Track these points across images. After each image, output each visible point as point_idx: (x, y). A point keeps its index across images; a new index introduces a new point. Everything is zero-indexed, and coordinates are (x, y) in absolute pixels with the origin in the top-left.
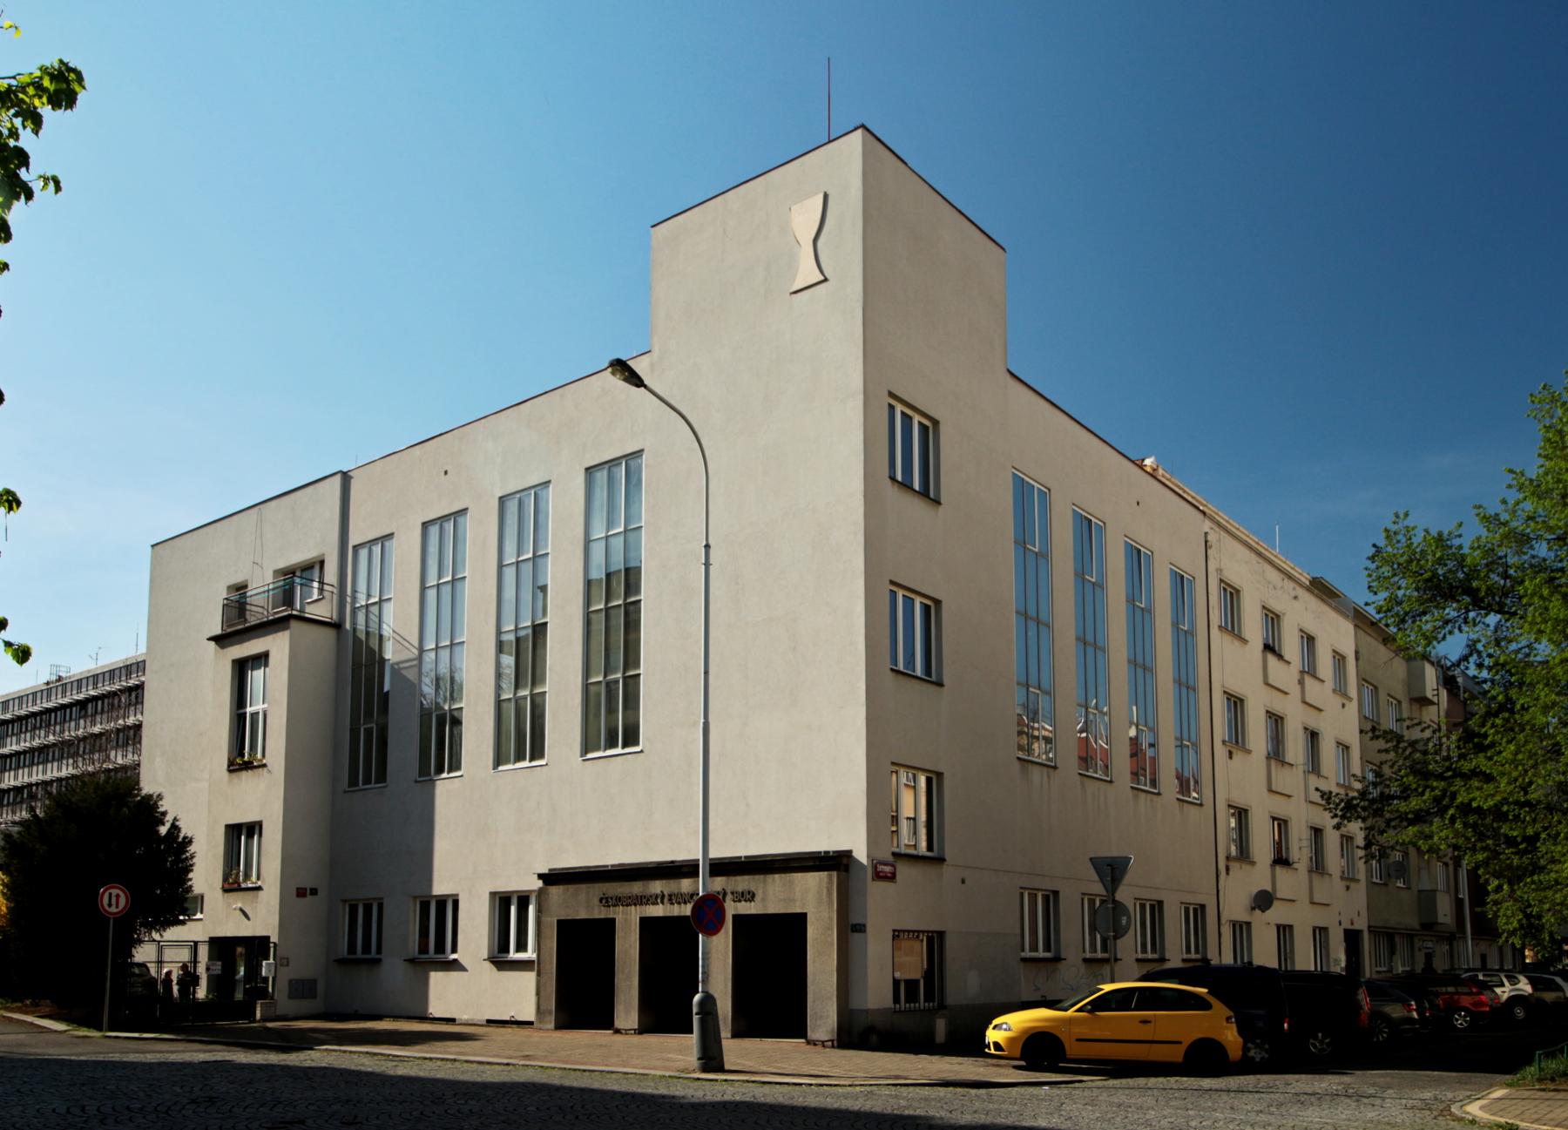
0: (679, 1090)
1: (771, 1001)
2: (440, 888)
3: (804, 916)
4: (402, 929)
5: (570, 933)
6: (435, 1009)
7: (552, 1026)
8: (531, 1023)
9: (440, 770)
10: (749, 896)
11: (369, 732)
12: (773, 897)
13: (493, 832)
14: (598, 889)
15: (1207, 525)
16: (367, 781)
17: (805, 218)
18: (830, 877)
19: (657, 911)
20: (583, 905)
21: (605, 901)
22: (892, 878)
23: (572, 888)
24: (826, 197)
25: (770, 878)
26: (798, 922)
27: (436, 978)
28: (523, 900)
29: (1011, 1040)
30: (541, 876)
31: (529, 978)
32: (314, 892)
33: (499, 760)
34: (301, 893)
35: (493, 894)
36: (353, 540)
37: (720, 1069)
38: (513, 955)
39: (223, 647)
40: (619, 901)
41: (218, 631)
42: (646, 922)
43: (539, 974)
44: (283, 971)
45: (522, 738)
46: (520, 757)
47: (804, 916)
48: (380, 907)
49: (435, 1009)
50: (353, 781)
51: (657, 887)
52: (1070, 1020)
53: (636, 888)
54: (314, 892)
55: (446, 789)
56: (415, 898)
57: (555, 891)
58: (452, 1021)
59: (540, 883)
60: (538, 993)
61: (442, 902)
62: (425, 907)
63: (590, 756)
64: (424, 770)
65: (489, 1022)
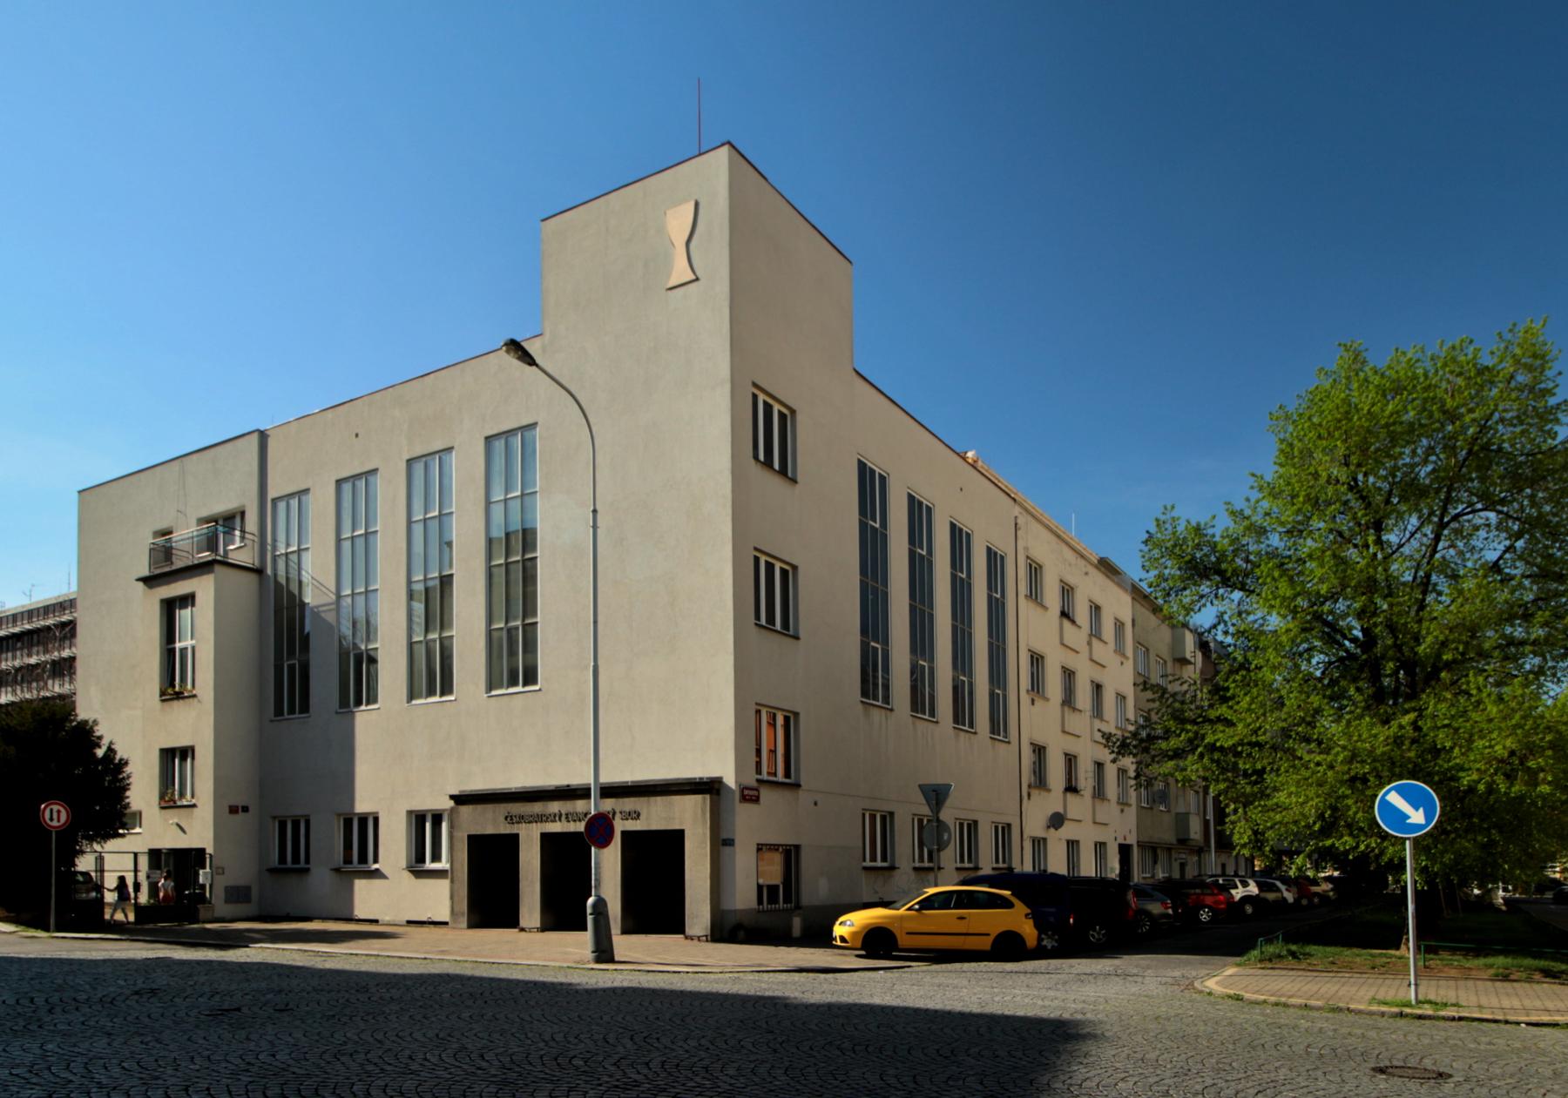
0: (575, 978)
1: (655, 901)
2: (361, 806)
3: (681, 832)
4: (327, 841)
5: (478, 845)
7: (465, 925)
9: (359, 703)
10: (636, 815)
11: (292, 668)
12: (655, 816)
13: (406, 759)
15: (1017, 510)
16: (292, 711)
17: (678, 222)
19: (555, 827)
20: (491, 822)
21: (510, 819)
22: (756, 800)
23: (480, 807)
24: (697, 204)
25: (653, 799)
26: (677, 837)
27: (360, 885)
28: (437, 818)
29: (854, 934)
30: (452, 797)
31: (443, 885)
32: (245, 809)
33: (412, 696)
34: (233, 810)
35: (410, 813)
36: (272, 493)
37: (611, 960)
38: (429, 865)
39: (151, 587)
40: (522, 819)
41: (145, 572)
42: (546, 838)
44: (217, 878)
45: (433, 675)
47: (681, 832)
49: (360, 912)
50: (279, 711)
51: (555, 807)
52: (901, 918)
53: (537, 808)
54: (245, 809)
55: (364, 718)
56: (274, 818)
57: (465, 810)
58: (376, 921)
59: (452, 803)
60: (452, 898)
61: (363, 819)
62: (348, 823)
64: (344, 703)
65: (409, 922)
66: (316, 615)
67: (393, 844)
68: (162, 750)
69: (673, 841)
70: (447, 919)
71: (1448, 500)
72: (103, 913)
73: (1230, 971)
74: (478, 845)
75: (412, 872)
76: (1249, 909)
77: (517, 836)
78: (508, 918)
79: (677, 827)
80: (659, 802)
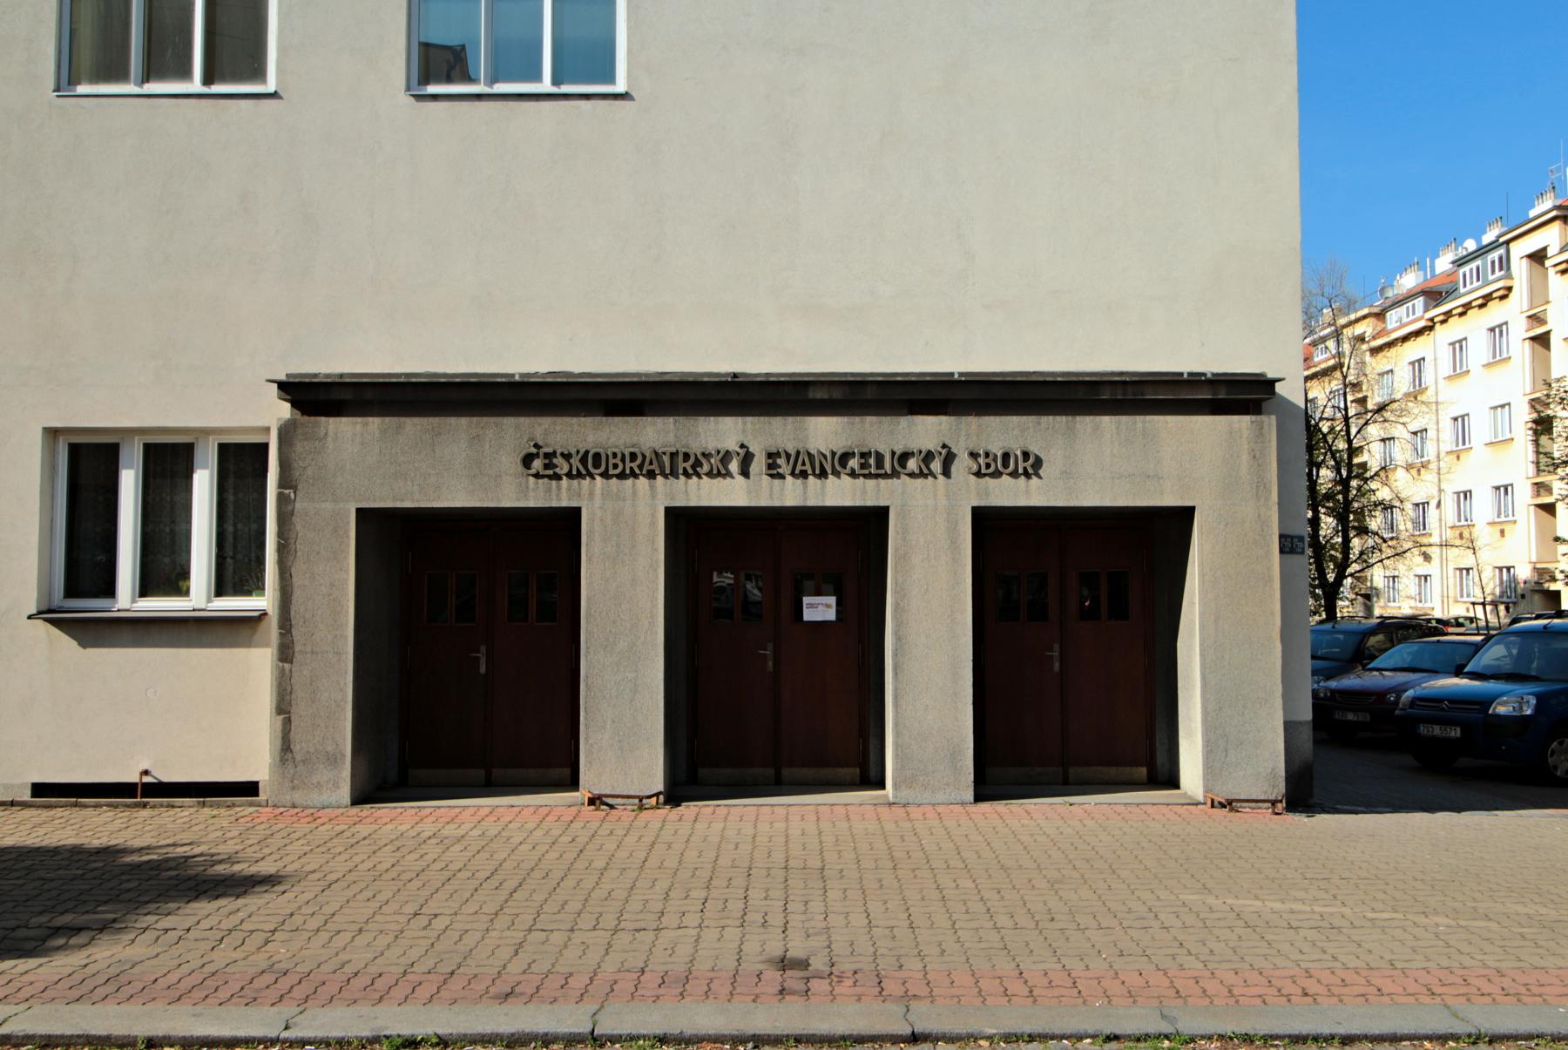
5: (398, 545)
8: (250, 789)
10: (1032, 466)
12: (1092, 468)
14: (512, 434)
18: (1260, 433)
19: (731, 493)
20: (471, 472)
23: (413, 426)
25: (1085, 423)
28: (241, 463)
31: (257, 663)
40: (591, 464)
42: (685, 526)
43: (286, 653)
46: (165, 58)
47: (886, 510)
51: (723, 432)
53: (654, 433)
57: (345, 434)
59: (285, 410)
60: (283, 707)
63: (432, 89)
65: (40, 790)
68: (45, 429)
69: (1152, 544)
70: (257, 765)
72: (478, 668)
73: (298, 527)
74: (398, 545)
76: (820, 609)
77: (571, 517)
78: (538, 750)
79: (882, 503)
80: (1104, 434)
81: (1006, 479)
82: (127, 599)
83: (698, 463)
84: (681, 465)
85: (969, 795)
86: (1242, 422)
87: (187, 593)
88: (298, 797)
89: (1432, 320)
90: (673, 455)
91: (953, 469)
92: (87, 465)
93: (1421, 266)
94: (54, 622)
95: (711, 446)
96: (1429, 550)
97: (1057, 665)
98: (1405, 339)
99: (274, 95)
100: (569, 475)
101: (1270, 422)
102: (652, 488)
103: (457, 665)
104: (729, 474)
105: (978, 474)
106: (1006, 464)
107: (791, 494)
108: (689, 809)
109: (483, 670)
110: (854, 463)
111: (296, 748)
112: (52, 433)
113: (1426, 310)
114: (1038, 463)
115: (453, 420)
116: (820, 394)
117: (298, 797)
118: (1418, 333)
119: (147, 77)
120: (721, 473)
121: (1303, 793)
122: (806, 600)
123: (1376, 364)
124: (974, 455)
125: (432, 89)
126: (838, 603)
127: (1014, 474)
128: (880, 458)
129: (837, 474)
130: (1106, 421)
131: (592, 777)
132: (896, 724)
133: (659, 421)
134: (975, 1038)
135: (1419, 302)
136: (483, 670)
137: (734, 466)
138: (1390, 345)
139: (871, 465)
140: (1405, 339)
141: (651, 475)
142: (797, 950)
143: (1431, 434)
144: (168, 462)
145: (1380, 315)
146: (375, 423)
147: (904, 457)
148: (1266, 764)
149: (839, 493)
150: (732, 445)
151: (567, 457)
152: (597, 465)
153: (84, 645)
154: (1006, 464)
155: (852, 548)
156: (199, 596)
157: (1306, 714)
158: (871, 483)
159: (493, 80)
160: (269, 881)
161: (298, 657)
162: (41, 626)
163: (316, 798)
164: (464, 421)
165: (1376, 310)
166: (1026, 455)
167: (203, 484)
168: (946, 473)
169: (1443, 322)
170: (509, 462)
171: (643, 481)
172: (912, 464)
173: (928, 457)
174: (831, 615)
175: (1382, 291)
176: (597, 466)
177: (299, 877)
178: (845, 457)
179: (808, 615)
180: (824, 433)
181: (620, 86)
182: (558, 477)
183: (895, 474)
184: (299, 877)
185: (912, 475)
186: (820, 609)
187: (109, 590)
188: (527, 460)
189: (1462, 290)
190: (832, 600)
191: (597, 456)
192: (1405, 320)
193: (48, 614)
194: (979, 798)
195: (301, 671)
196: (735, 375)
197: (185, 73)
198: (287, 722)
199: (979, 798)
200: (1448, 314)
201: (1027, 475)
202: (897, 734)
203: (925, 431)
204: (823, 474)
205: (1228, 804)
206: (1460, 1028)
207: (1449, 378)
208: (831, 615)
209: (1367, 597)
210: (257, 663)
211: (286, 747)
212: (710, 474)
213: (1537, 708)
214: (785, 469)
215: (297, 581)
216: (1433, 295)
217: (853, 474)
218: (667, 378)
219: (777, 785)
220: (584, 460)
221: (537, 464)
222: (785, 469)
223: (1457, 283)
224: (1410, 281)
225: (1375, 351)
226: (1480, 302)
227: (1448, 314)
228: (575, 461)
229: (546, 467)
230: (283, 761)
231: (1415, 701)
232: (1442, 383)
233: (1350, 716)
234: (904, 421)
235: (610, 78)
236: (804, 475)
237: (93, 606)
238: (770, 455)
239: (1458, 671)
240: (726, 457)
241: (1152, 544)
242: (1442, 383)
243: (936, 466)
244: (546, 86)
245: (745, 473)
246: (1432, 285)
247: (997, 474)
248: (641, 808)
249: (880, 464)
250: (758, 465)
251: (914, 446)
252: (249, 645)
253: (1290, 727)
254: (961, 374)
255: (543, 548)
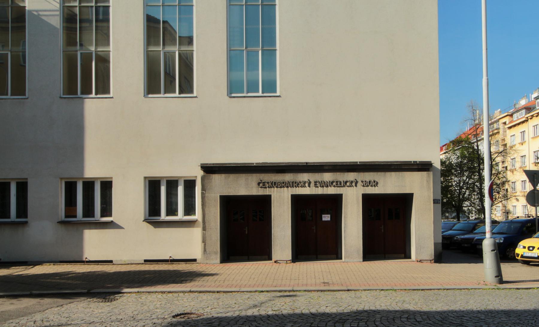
1: (316, 237)
5: (229, 204)
6: (89, 254)
7: (219, 260)
8: (195, 260)
9: (87, 91)
10: (376, 184)
12: (389, 185)
14: (254, 178)
20: (245, 187)
23: (232, 176)
25: (388, 174)
28: (190, 185)
31: (197, 232)
35: (145, 178)
40: (274, 185)
43: (204, 229)
46: (170, 89)
48: (22, 187)
49: (89, 254)
51: (304, 177)
53: (288, 177)
56: (61, 179)
57: (217, 179)
59: (201, 173)
60: (204, 241)
61: (89, 185)
62: (70, 187)
63: (233, 95)
64: (70, 88)
65: (145, 261)
66: (37, 17)
67: (129, 201)
69: (404, 202)
71: (478, 188)
74: (229, 204)
75: (150, 223)
76: (326, 218)
81: (370, 187)
82: (163, 216)
83: (298, 184)
84: (294, 185)
85: (362, 260)
86: (424, 173)
87: (177, 215)
88: (208, 261)
89: (527, 118)
90: (293, 182)
91: (358, 185)
92: (153, 185)
93: (527, 97)
94: (148, 222)
95: (301, 180)
96: (518, 198)
97: (383, 231)
98: (519, 124)
99: (196, 97)
100: (269, 187)
101: (431, 173)
102: (288, 190)
103: (243, 231)
104: (305, 187)
105: (363, 186)
106: (370, 184)
107: (320, 191)
108: (298, 264)
109: (247, 233)
110: (334, 184)
111: (207, 250)
112: (145, 178)
113: (526, 114)
114: (377, 183)
115: (241, 175)
116: (326, 168)
117: (208, 261)
118: (523, 122)
119: (165, 93)
120: (304, 186)
121: (439, 258)
122: (323, 216)
123: (510, 133)
124: (362, 182)
125: (233, 95)
126: (515, 246)
127: (372, 186)
128: (340, 182)
129: (331, 186)
130: (393, 173)
131: (275, 257)
132: (345, 244)
133: (289, 174)
134: (359, 290)
135: (524, 111)
136: (247, 233)
137: (307, 185)
138: (515, 126)
139: (339, 184)
140: (519, 124)
141: (287, 187)
142: (326, 281)
143: (527, 156)
144: (172, 184)
145: (511, 115)
146: (223, 175)
147: (346, 182)
148: (429, 251)
149: (331, 191)
150: (306, 180)
151: (268, 183)
152: (275, 185)
153: (155, 227)
154: (370, 184)
155: (334, 203)
156: (181, 215)
157: (440, 240)
158: (338, 188)
159: (248, 92)
160: (212, 275)
161: (207, 230)
162: (145, 223)
163: (212, 262)
164: (244, 175)
165: (510, 114)
166: (374, 181)
167: (181, 190)
168: (356, 186)
169: (531, 119)
170: (255, 184)
171: (286, 188)
172: (348, 184)
173: (352, 182)
174: (329, 219)
175: (515, 105)
176: (275, 185)
177: (221, 274)
178: (332, 182)
179: (324, 219)
180: (327, 177)
181: (278, 94)
182: (266, 188)
183: (344, 186)
184: (221, 274)
185: (348, 186)
186: (326, 218)
187: (159, 215)
188: (259, 184)
189: (537, 108)
190: (329, 216)
191: (275, 183)
192: (519, 117)
193: (145, 220)
194: (363, 261)
195: (208, 233)
196: (307, 163)
197: (174, 92)
198: (205, 245)
199: (363, 261)
200: (532, 116)
201: (375, 186)
202: (345, 246)
203: (351, 176)
204: (327, 186)
205: (420, 261)
206: (442, 288)
207: (533, 138)
208: (329, 219)
209: (508, 213)
210: (197, 232)
211: (205, 250)
212: (301, 187)
213: (504, 241)
214: (318, 185)
215: (206, 212)
216: (528, 109)
217: (334, 186)
218: (290, 164)
219: (317, 259)
220: (272, 184)
221: (261, 185)
222: (318, 185)
223: (535, 104)
224: (523, 102)
225: (510, 128)
226: (536, 115)
227: (532, 116)
228: (270, 184)
229: (263, 185)
230: (204, 253)
231: (477, 239)
232: (530, 139)
233: (466, 245)
234: (346, 174)
235: (275, 92)
236: (323, 187)
237: (156, 218)
238: (315, 182)
239: (451, 230)
240: (305, 183)
241: (404, 202)
242: (530, 139)
243: (354, 184)
244: (260, 94)
245: (309, 186)
246: (529, 105)
247: (368, 186)
248: (287, 263)
249: (340, 184)
250: (312, 184)
251: (348, 180)
252: (193, 227)
253: (436, 244)
254: (360, 162)
255: (263, 204)
